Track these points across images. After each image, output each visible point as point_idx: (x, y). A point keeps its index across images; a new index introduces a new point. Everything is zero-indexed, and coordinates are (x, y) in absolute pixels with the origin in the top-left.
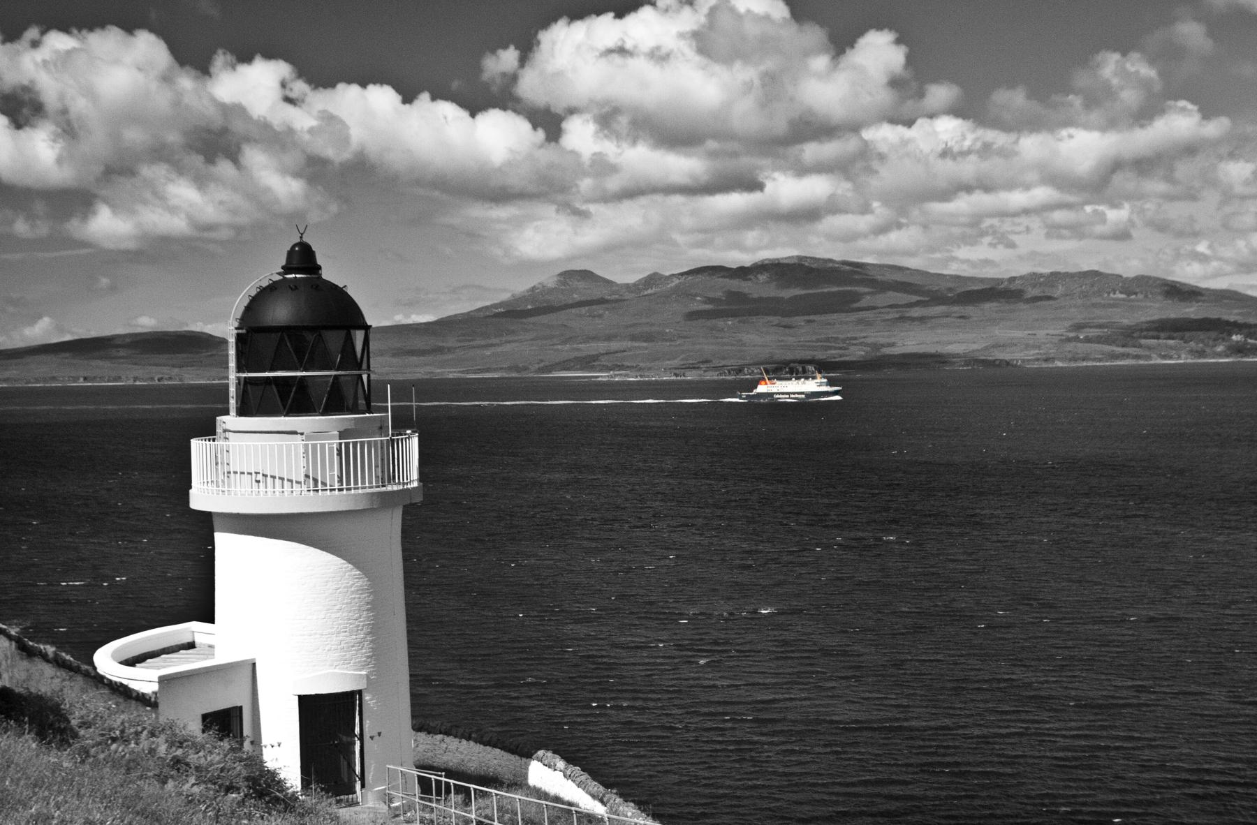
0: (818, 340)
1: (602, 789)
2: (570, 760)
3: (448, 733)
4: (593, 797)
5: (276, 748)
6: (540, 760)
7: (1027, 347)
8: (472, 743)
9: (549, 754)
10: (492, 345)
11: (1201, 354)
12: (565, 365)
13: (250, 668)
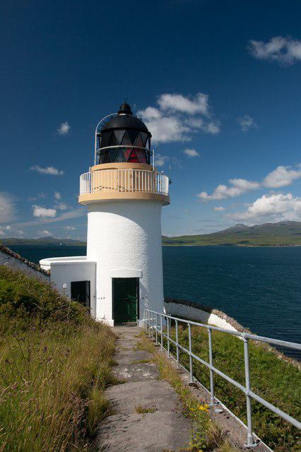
1: (242, 327)
9: (221, 312)
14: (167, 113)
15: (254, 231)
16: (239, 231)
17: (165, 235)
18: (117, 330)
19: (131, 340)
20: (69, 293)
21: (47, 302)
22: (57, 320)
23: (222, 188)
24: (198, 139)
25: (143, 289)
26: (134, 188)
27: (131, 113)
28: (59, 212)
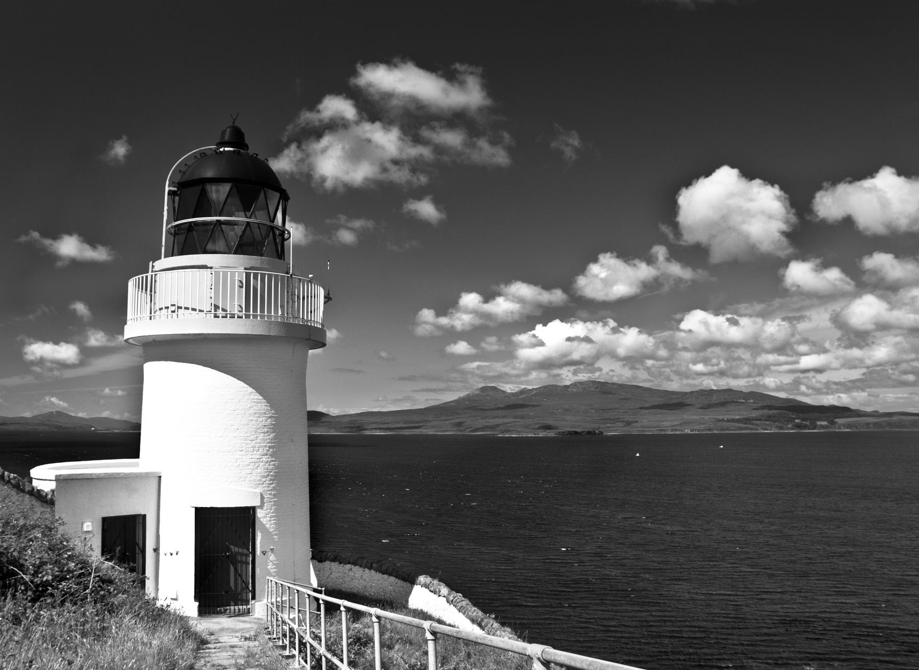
1: (480, 614)
2: (453, 587)
3: (355, 564)
4: (473, 621)
6: (426, 586)
7: (700, 424)
8: (373, 572)
9: (436, 582)
11: (781, 428)
12: (483, 429)
13: (156, 480)
14: (373, 108)
15: (518, 404)
16: (486, 401)
17: (320, 409)
18: (203, 626)
19: (232, 647)
20: (96, 542)
21: (43, 563)
22: (63, 603)
23: (470, 299)
24: (447, 179)
25: (265, 530)
26: (247, 309)
27: (246, 147)
28: (87, 353)
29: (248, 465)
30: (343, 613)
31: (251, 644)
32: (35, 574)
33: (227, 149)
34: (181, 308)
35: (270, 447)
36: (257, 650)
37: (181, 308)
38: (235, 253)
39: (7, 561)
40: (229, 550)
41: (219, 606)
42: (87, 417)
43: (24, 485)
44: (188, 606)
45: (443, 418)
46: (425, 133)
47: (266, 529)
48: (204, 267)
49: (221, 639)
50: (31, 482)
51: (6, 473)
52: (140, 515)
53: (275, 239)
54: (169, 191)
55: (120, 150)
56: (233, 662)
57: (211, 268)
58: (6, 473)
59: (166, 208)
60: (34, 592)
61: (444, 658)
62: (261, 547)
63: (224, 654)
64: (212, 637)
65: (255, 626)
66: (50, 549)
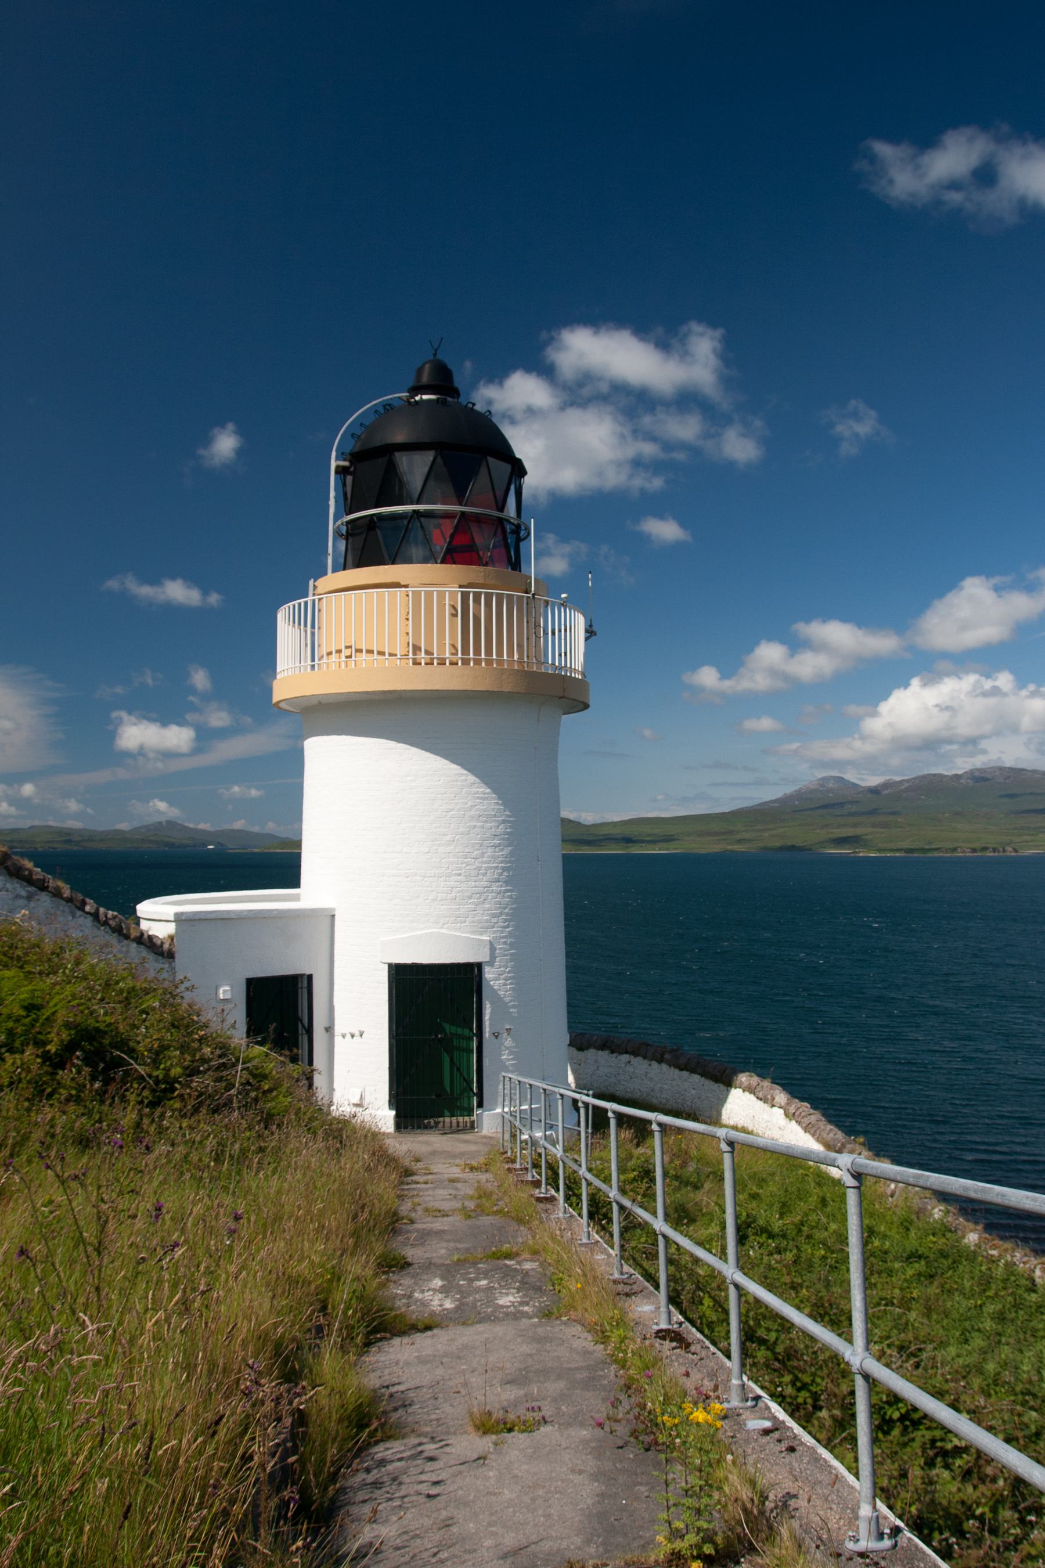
0: (1015, 829)
1: (840, 1135)
5: (357, 1039)
6: (750, 1090)
8: (664, 1066)
9: (766, 1083)
10: (769, 830)
13: (328, 920)
16: (832, 803)
18: (406, 1146)
19: (452, 1181)
20: (239, 1015)
21: (164, 1048)
22: (196, 1110)
24: (688, 482)
25: (497, 1000)
27: (455, 392)
28: (205, 736)
29: (470, 897)
30: (657, 1135)
31: (483, 1177)
32: (156, 1063)
33: (425, 397)
34: (360, 651)
35: (504, 869)
36: (490, 1187)
37: (360, 651)
38: (442, 562)
39: (110, 1044)
40: (442, 1030)
41: (426, 1117)
42: (212, 829)
43: (129, 929)
44: (382, 1116)
45: (759, 827)
46: (647, 420)
47: (500, 998)
48: (397, 585)
49: (434, 1168)
50: (138, 924)
51: (102, 910)
52: (302, 975)
53: (505, 539)
54: (337, 467)
55: (226, 444)
56: (459, 1205)
57: (406, 586)
58: (102, 910)
59: (332, 494)
60: (153, 1091)
61: (784, 1205)
62: (490, 1025)
63: (441, 1192)
64: (420, 1165)
65: (485, 1149)
66: (173, 1025)
